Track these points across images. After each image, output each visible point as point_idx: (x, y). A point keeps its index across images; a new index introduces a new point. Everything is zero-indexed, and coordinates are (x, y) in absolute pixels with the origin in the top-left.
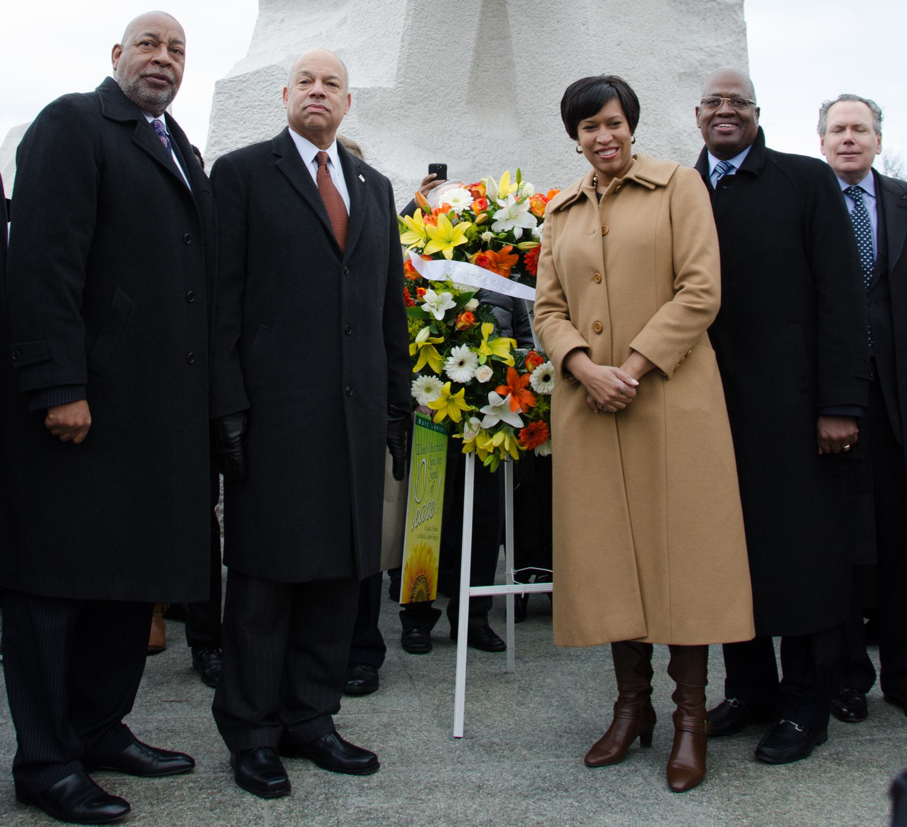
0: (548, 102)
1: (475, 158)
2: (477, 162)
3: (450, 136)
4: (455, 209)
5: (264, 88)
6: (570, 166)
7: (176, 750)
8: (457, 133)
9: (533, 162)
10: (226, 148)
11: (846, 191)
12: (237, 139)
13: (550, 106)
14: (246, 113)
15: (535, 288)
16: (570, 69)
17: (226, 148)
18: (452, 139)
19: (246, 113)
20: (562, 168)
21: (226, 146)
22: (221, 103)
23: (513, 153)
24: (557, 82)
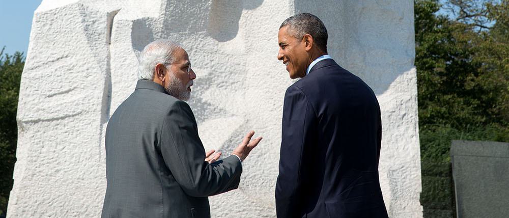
0: (264, 30)
1: (212, 68)
2: (214, 70)
3: (196, 52)
4: (466, 88)
5: (70, 19)
6: (276, 77)
7: (247, 158)
8: (200, 50)
9: (253, 71)
10: (41, 61)
11: (201, 103)
12: (49, 55)
13: (265, 33)
14: (56, 36)
15: (327, 54)
16: (279, 9)
17: (41, 61)
18: (197, 53)
19: (56, 36)
20: (271, 78)
21: (41, 60)
22: (39, 29)
23: (239, 64)
24: (271, 17)
